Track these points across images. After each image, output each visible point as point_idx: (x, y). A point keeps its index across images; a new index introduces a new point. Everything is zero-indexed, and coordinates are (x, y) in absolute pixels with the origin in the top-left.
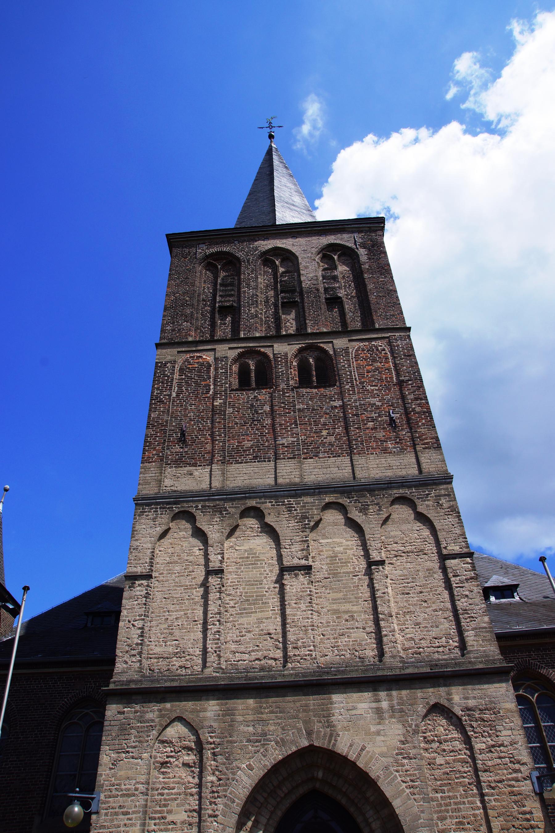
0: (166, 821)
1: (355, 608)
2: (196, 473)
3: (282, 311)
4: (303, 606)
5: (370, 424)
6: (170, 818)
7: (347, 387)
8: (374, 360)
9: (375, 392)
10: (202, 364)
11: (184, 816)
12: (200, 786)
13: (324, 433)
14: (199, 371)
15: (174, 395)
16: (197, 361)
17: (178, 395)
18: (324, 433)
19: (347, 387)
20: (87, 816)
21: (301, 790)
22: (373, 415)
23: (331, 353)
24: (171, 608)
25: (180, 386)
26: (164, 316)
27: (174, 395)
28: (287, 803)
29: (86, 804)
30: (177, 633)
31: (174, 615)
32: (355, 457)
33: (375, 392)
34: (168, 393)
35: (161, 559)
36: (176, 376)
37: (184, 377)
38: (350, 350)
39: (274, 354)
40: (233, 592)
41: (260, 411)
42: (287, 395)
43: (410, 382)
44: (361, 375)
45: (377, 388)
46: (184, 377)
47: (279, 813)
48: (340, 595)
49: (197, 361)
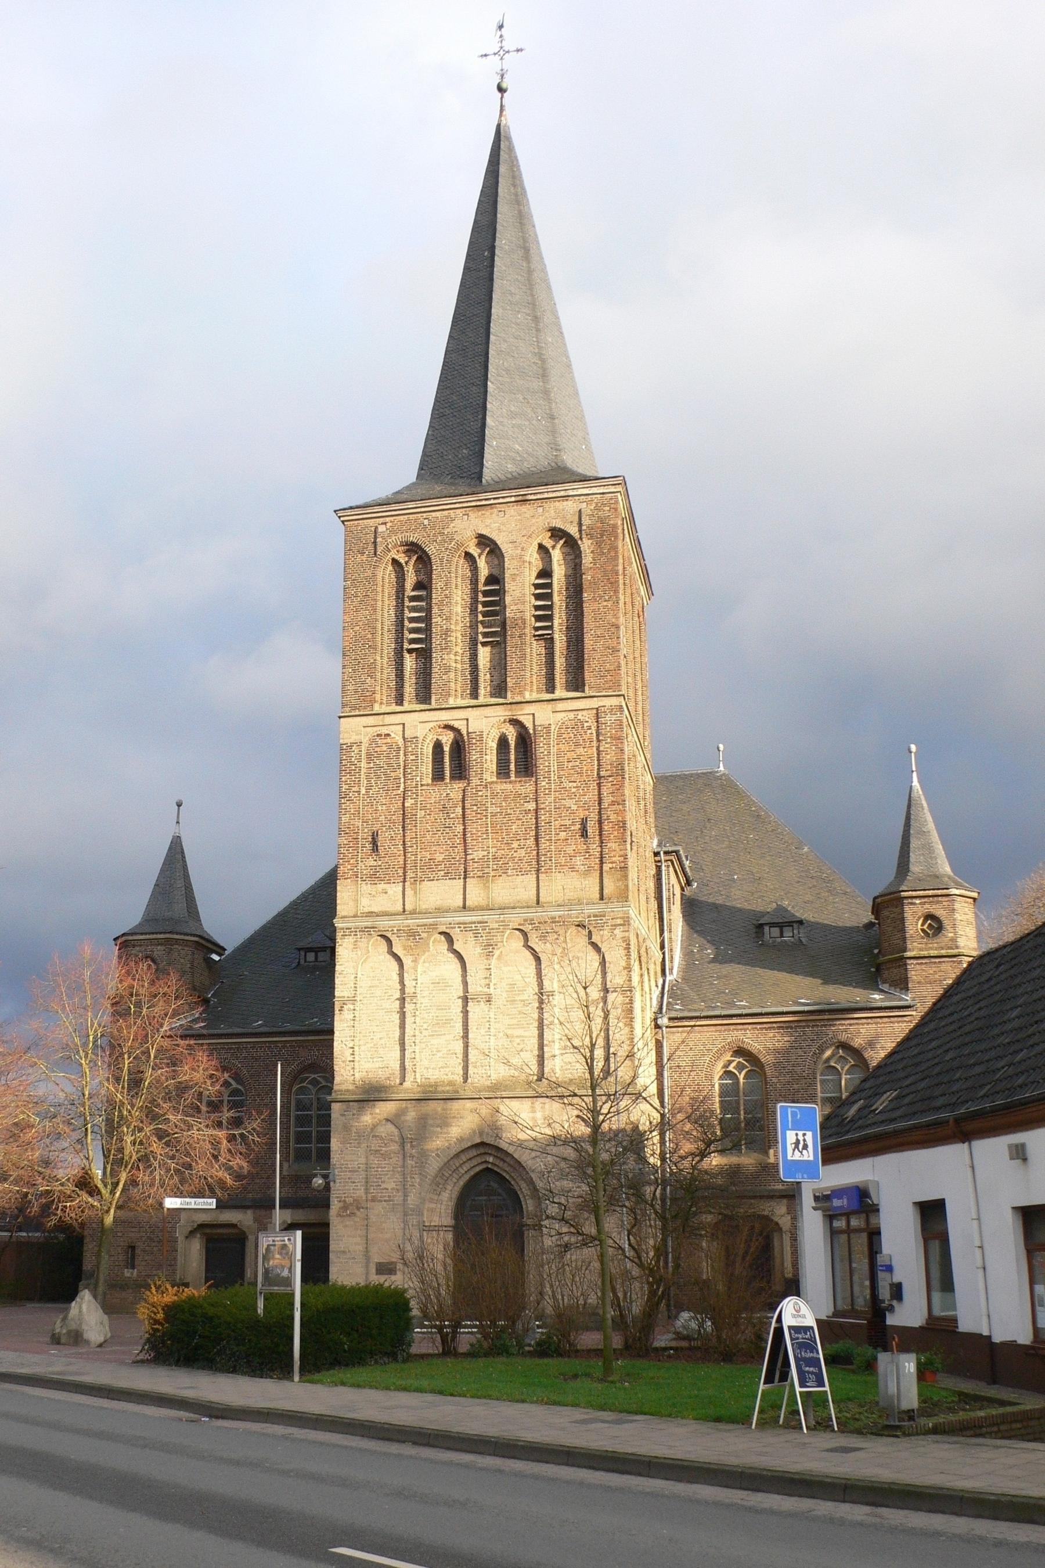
0: (48, 1172)
1: (526, 1034)
2: (390, 892)
3: (301, 1375)
4: (483, 1031)
5: (563, 835)
6: (384, 1186)
7: (544, 783)
8: (577, 744)
9: (574, 790)
10: (390, 747)
11: (393, 1185)
12: (403, 1166)
13: (515, 845)
14: (388, 758)
15: (363, 791)
16: (385, 741)
17: (368, 790)
18: (515, 845)
19: (544, 783)
20: (327, 1184)
21: (478, 1169)
22: (568, 823)
23: (531, 731)
24: (375, 1029)
25: (369, 780)
26: (344, 667)
27: (363, 791)
28: (467, 1177)
29: (325, 1177)
30: (381, 1051)
31: (379, 1036)
32: (542, 876)
33: (574, 790)
34: (355, 789)
35: (364, 984)
36: (363, 764)
37: (372, 765)
38: (552, 728)
39: (468, 733)
40: (426, 1015)
41: (452, 816)
42: (480, 793)
43: (611, 779)
44: (561, 767)
45: (575, 785)
46: (372, 765)
47: (462, 1183)
48: (515, 1021)
49: (385, 741)
